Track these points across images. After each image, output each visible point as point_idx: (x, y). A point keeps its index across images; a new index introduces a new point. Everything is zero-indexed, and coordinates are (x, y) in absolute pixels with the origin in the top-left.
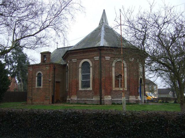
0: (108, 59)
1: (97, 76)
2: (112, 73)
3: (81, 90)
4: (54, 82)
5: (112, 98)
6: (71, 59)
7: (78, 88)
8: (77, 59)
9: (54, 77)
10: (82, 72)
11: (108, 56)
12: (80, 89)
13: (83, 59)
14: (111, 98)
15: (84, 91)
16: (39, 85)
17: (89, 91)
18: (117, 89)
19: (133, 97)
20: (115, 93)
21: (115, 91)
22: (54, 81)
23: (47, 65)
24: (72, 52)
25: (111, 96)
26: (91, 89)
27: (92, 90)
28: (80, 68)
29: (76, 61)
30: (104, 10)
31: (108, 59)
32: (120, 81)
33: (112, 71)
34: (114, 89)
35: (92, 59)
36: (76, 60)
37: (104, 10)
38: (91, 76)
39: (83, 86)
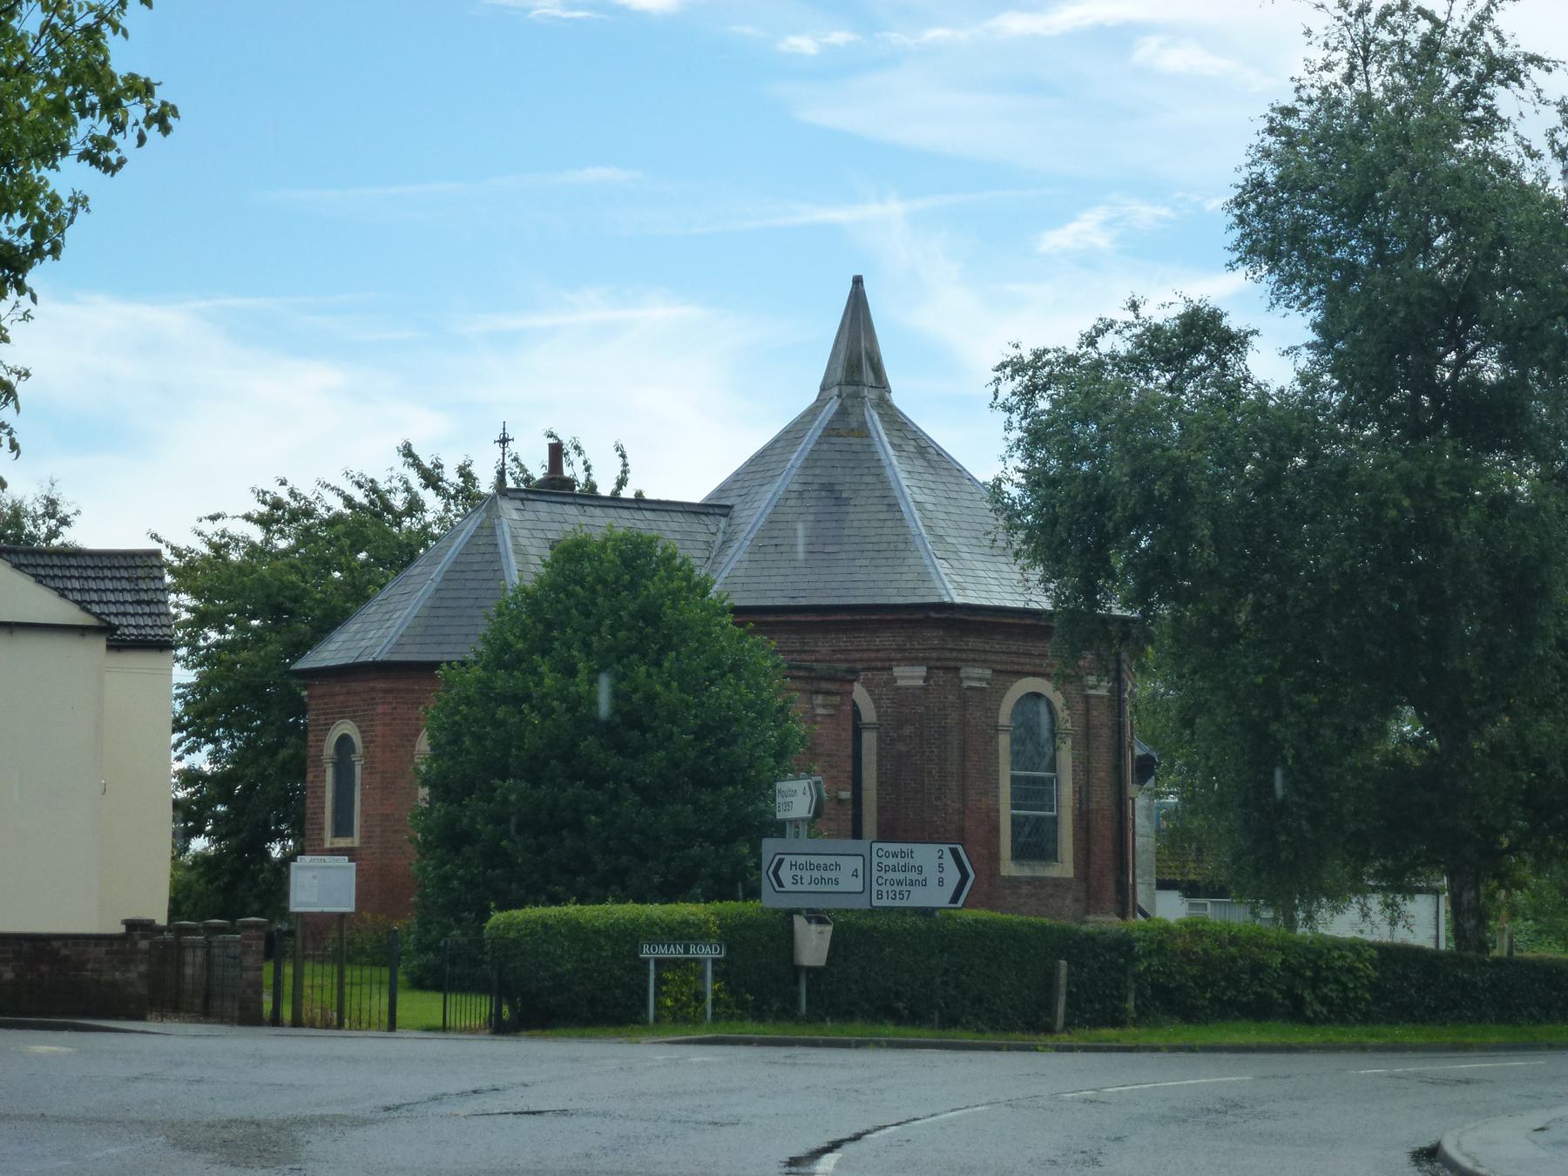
0: (913, 678)
3: (1016, 878)
6: (956, 659)
7: (995, 858)
8: (994, 671)
10: (1017, 759)
11: (984, 663)
12: (1008, 868)
13: (1020, 674)
15: (1032, 881)
23: (825, 685)
24: (972, 618)
26: (1064, 868)
29: (984, 685)
30: (858, 281)
31: (913, 678)
35: (1072, 689)
37: (858, 281)
38: (1066, 791)
39: (1019, 854)
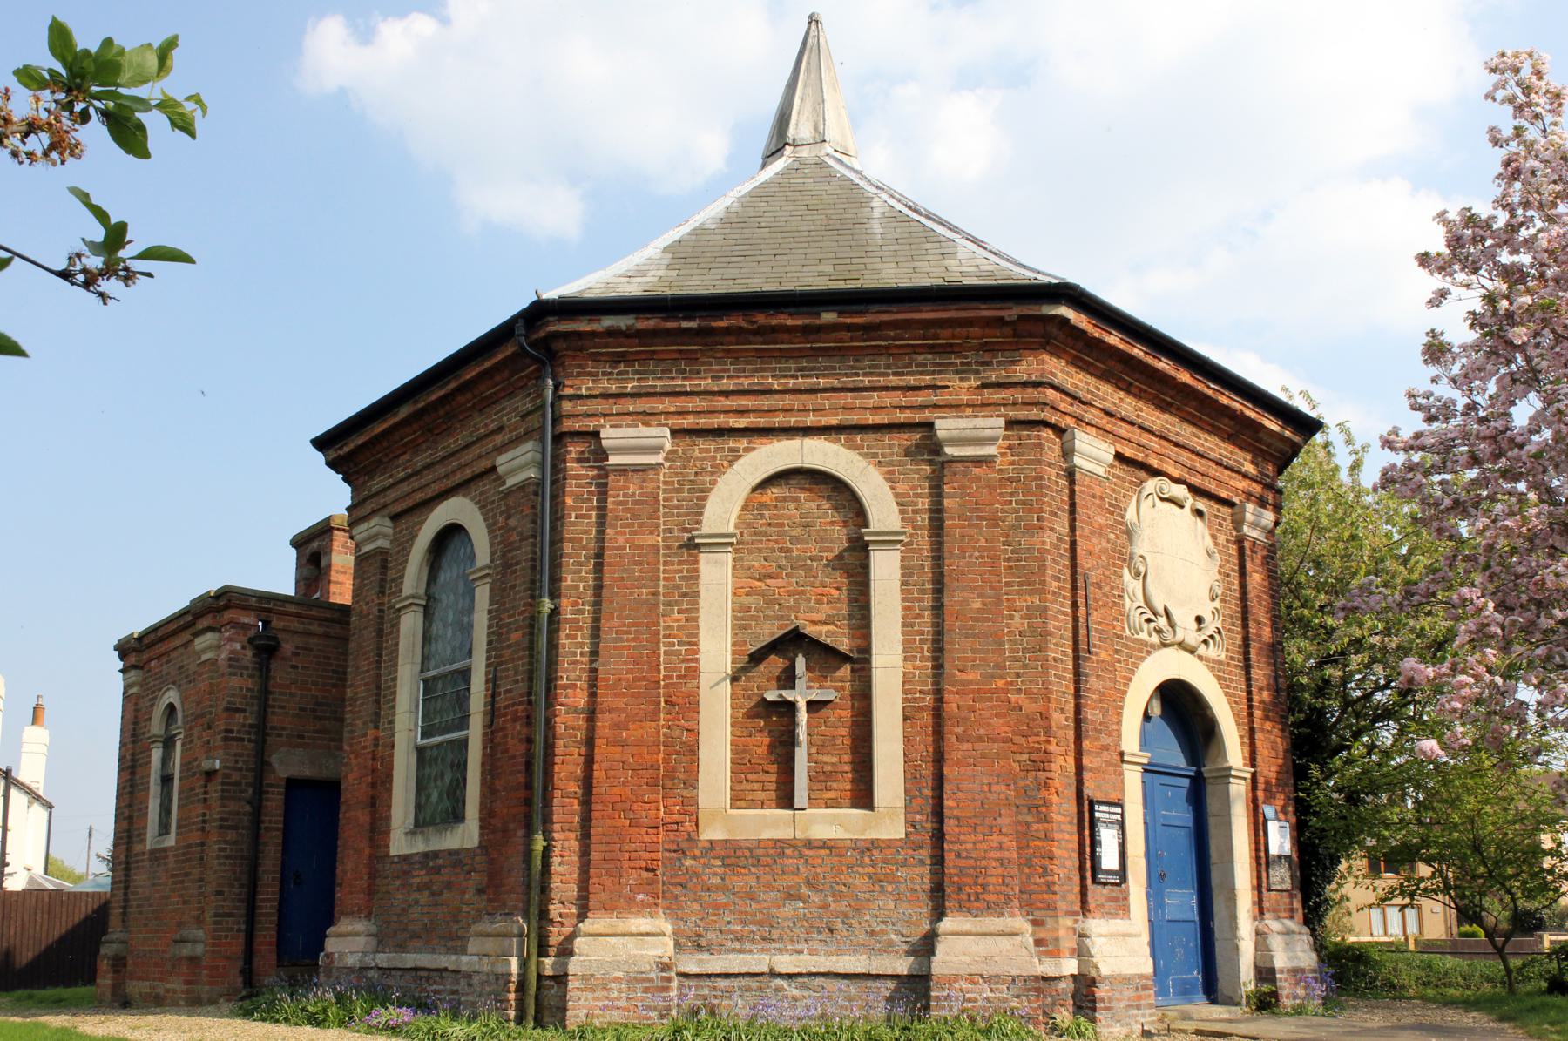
1: (513, 686)
2: (692, 621)
4: (260, 789)
5: (691, 942)
9: (261, 730)
14: (665, 948)
16: (164, 829)
17: (455, 858)
18: (769, 824)
19: (993, 923)
20: (737, 882)
21: (733, 854)
22: (261, 766)
25: (674, 911)
27: (480, 846)
28: (718, 543)
32: (803, 716)
33: (694, 607)
34: (711, 832)
36: (659, 434)
